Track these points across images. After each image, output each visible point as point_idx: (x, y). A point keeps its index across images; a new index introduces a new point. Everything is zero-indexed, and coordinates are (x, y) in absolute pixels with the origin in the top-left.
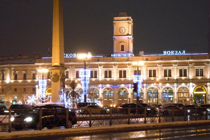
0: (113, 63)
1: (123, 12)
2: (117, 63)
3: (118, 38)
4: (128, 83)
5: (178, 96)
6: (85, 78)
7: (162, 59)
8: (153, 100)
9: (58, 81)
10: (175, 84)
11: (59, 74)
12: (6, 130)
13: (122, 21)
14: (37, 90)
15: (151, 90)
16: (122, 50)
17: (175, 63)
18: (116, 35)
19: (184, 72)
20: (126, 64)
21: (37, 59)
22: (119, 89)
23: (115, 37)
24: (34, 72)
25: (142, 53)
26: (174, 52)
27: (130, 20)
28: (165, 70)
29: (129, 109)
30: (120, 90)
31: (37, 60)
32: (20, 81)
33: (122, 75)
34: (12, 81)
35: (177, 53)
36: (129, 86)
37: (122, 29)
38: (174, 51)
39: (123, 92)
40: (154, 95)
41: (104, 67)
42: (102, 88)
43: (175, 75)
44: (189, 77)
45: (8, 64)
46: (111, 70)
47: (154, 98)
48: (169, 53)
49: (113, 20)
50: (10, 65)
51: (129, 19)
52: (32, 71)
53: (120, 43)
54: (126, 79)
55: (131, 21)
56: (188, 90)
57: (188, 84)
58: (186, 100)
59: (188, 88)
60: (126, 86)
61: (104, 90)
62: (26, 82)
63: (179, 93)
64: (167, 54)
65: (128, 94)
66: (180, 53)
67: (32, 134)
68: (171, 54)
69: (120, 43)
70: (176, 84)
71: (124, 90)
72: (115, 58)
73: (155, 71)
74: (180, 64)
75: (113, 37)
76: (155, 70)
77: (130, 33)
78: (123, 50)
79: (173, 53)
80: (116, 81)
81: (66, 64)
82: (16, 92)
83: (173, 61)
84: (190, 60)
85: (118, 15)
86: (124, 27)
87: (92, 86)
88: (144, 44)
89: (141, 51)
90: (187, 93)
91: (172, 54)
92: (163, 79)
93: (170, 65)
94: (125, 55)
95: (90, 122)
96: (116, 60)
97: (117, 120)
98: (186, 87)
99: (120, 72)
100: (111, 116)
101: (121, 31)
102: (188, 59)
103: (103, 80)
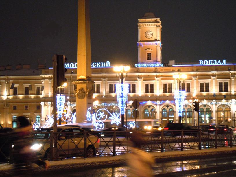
0: (137, 74)
1: (150, 12)
2: (143, 74)
3: (144, 44)
4: (156, 100)
5: (217, 116)
6: (122, 94)
7: (197, 71)
8: (186, 121)
9: (84, 98)
10: (214, 100)
11: (85, 89)
12: (110, 152)
13: (148, 24)
14: (43, 107)
15: (166, 108)
16: (148, 59)
17: (214, 75)
18: (142, 40)
19: (225, 86)
20: (154, 77)
21: (42, 69)
22: (144, 108)
23: (140, 43)
24: (39, 85)
25: (172, 62)
26: (212, 62)
27: (159, 22)
28: (201, 84)
29: (182, 131)
30: (147, 108)
31: (43, 70)
32: (21, 97)
33: (203, 89)
34: (11, 97)
35: (216, 63)
36: (157, 103)
37: (148, 33)
38: (212, 61)
39: (149, 110)
40: (188, 114)
41: (144, 80)
42: (160, 105)
43: (214, 90)
44: (231, 92)
45: (5, 75)
46: (134, 84)
47: (187, 117)
48: (206, 62)
49: (138, 22)
50: (9, 77)
51: (157, 21)
52: (36, 85)
53: (146, 50)
54: (153, 94)
55: (159, 24)
56: (230, 108)
57: (229, 101)
58: (227, 121)
59: (230, 105)
60: (153, 103)
61: (162, 108)
62: (28, 98)
63: (218, 111)
64: (204, 64)
65: (156, 112)
66: (220, 63)
67: (163, 155)
68: (208, 64)
69: (146, 50)
70: (215, 100)
71: (151, 108)
72: (140, 69)
73: (226, 84)
74: (220, 77)
75: (138, 43)
76: (189, 84)
77: (159, 38)
78: (149, 58)
79: (211, 63)
80: (141, 96)
81: (93, 75)
82: (14, 110)
83: (211, 73)
84: (232, 72)
85: (143, 17)
86: (151, 31)
87: (111, 103)
88: (176, 51)
89: (172, 60)
90: (229, 112)
91: (209, 65)
92: (199, 95)
93: (208, 77)
94: (152, 65)
95: (182, 145)
96: (141, 70)
97: (122, 147)
98: (227, 104)
99: (147, 85)
100: (182, 137)
101: (148, 35)
102: (229, 70)
103: (143, 95)
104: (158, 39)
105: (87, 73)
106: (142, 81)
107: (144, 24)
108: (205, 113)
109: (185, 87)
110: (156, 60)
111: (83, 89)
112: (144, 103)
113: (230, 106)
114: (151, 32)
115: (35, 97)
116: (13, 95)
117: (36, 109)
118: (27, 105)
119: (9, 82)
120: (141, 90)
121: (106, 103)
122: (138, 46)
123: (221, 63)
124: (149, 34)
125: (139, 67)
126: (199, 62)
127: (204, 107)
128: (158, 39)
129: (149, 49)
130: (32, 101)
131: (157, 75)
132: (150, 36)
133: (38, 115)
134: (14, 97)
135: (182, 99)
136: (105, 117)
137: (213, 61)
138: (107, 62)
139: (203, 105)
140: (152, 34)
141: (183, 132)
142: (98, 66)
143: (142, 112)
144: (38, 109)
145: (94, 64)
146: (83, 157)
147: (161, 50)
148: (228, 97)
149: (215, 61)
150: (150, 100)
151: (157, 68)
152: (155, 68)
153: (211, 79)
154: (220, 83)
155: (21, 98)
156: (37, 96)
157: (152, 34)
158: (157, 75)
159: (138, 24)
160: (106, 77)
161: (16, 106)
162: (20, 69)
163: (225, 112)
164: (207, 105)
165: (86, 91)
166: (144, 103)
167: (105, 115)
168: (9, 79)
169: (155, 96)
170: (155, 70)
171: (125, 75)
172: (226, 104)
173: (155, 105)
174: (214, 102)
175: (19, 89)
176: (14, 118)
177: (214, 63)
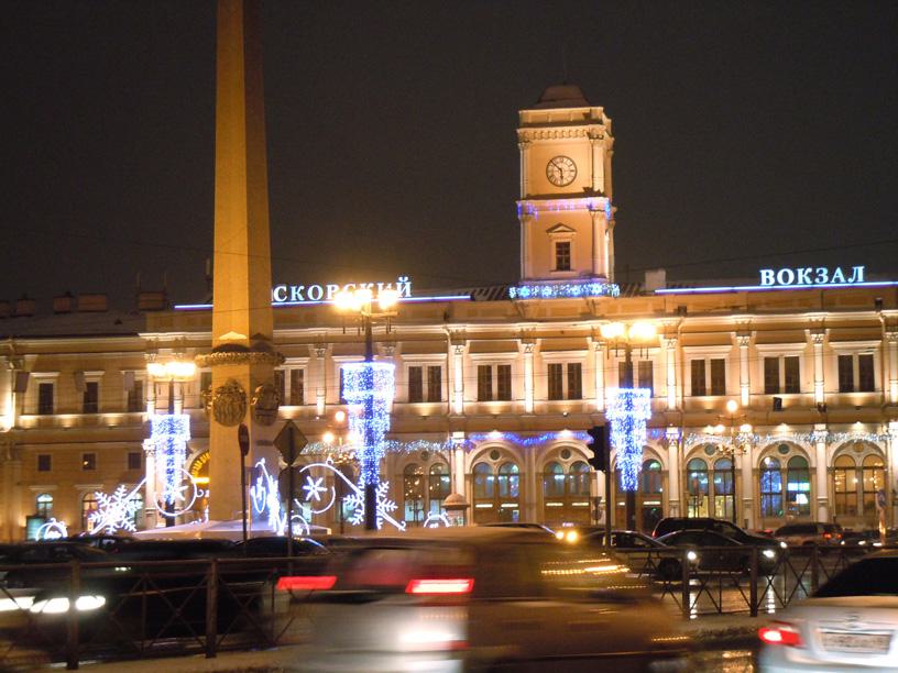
0: (517, 327)
2: (540, 327)
3: (542, 208)
7: (751, 309)
11: (246, 386)
13: (560, 129)
16: (560, 268)
17: (818, 328)
18: (533, 194)
21: (150, 310)
23: (528, 203)
26: (809, 275)
31: (150, 315)
32: (67, 419)
34: (29, 420)
35: (826, 279)
37: (560, 165)
39: (567, 468)
41: (473, 350)
42: (467, 448)
43: (819, 386)
44: (887, 394)
48: (786, 277)
49: (517, 123)
50: (19, 342)
51: (594, 117)
53: (550, 230)
54: (581, 405)
56: (884, 458)
57: (879, 429)
59: (882, 446)
62: (95, 423)
64: (777, 283)
65: (662, 474)
66: (842, 280)
68: (796, 282)
69: (550, 230)
70: (823, 426)
73: (719, 366)
74: (841, 332)
75: (519, 204)
76: (722, 361)
77: (599, 186)
79: (808, 280)
81: (279, 333)
82: (43, 473)
85: (539, 101)
88: (669, 238)
89: (655, 269)
93: (794, 334)
94: (576, 290)
96: (531, 313)
101: (557, 175)
102: (879, 306)
103: (541, 408)
104: (596, 190)
105: (251, 321)
106: (536, 351)
107: (549, 129)
108: (785, 476)
109: (633, 373)
110: (590, 268)
111: (236, 383)
112: (545, 437)
113: (883, 449)
114: (569, 162)
115: (120, 418)
116: (40, 413)
117: (126, 465)
118: (47, 454)
119: (21, 361)
120: (674, 383)
121: (396, 440)
122: (519, 217)
123: (846, 279)
124: (560, 169)
125: (522, 298)
126: (760, 275)
127: (493, 458)
128: (596, 190)
129: (560, 228)
130: (113, 435)
131: (522, 331)
132: (567, 177)
133: (45, 493)
134: (39, 420)
135: (636, 422)
136: (325, 497)
137: (814, 271)
138: (401, 279)
139: (776, 443)
140: (573, 168)
141: (214, 568)
142: (294, 298)
143: (537, 474)
144: (134, 467)
145: (281, 292)
146: (65, 665)
147: (611, 230)
148: (879, 413)
149: (821, 272)
150: (569, 429)
151: (593, 301)
152: (587, 304)
153: (731, 344)
154: (841, 358)
155: (67, 424)
156: (130, 418)
157: (573, 168)
158: (522, 331)
159: (519, 131)
160: (396, 341)
161: (48, 458)
162: (69, 312)
163: (865, 471)
164: (792, 443)
165: (248, 391)
166: (545, 437)
167: (325, 490)
168: (21, 352)
169: (589, 410)
170: (588, 311)
171: (378, 330)
172: (866, 441)
173: (661, 447)
174: (820, 434)
175: (59, 388)
176: (41, 506)
177: (817, 280)
